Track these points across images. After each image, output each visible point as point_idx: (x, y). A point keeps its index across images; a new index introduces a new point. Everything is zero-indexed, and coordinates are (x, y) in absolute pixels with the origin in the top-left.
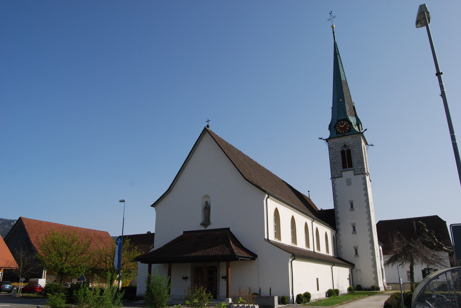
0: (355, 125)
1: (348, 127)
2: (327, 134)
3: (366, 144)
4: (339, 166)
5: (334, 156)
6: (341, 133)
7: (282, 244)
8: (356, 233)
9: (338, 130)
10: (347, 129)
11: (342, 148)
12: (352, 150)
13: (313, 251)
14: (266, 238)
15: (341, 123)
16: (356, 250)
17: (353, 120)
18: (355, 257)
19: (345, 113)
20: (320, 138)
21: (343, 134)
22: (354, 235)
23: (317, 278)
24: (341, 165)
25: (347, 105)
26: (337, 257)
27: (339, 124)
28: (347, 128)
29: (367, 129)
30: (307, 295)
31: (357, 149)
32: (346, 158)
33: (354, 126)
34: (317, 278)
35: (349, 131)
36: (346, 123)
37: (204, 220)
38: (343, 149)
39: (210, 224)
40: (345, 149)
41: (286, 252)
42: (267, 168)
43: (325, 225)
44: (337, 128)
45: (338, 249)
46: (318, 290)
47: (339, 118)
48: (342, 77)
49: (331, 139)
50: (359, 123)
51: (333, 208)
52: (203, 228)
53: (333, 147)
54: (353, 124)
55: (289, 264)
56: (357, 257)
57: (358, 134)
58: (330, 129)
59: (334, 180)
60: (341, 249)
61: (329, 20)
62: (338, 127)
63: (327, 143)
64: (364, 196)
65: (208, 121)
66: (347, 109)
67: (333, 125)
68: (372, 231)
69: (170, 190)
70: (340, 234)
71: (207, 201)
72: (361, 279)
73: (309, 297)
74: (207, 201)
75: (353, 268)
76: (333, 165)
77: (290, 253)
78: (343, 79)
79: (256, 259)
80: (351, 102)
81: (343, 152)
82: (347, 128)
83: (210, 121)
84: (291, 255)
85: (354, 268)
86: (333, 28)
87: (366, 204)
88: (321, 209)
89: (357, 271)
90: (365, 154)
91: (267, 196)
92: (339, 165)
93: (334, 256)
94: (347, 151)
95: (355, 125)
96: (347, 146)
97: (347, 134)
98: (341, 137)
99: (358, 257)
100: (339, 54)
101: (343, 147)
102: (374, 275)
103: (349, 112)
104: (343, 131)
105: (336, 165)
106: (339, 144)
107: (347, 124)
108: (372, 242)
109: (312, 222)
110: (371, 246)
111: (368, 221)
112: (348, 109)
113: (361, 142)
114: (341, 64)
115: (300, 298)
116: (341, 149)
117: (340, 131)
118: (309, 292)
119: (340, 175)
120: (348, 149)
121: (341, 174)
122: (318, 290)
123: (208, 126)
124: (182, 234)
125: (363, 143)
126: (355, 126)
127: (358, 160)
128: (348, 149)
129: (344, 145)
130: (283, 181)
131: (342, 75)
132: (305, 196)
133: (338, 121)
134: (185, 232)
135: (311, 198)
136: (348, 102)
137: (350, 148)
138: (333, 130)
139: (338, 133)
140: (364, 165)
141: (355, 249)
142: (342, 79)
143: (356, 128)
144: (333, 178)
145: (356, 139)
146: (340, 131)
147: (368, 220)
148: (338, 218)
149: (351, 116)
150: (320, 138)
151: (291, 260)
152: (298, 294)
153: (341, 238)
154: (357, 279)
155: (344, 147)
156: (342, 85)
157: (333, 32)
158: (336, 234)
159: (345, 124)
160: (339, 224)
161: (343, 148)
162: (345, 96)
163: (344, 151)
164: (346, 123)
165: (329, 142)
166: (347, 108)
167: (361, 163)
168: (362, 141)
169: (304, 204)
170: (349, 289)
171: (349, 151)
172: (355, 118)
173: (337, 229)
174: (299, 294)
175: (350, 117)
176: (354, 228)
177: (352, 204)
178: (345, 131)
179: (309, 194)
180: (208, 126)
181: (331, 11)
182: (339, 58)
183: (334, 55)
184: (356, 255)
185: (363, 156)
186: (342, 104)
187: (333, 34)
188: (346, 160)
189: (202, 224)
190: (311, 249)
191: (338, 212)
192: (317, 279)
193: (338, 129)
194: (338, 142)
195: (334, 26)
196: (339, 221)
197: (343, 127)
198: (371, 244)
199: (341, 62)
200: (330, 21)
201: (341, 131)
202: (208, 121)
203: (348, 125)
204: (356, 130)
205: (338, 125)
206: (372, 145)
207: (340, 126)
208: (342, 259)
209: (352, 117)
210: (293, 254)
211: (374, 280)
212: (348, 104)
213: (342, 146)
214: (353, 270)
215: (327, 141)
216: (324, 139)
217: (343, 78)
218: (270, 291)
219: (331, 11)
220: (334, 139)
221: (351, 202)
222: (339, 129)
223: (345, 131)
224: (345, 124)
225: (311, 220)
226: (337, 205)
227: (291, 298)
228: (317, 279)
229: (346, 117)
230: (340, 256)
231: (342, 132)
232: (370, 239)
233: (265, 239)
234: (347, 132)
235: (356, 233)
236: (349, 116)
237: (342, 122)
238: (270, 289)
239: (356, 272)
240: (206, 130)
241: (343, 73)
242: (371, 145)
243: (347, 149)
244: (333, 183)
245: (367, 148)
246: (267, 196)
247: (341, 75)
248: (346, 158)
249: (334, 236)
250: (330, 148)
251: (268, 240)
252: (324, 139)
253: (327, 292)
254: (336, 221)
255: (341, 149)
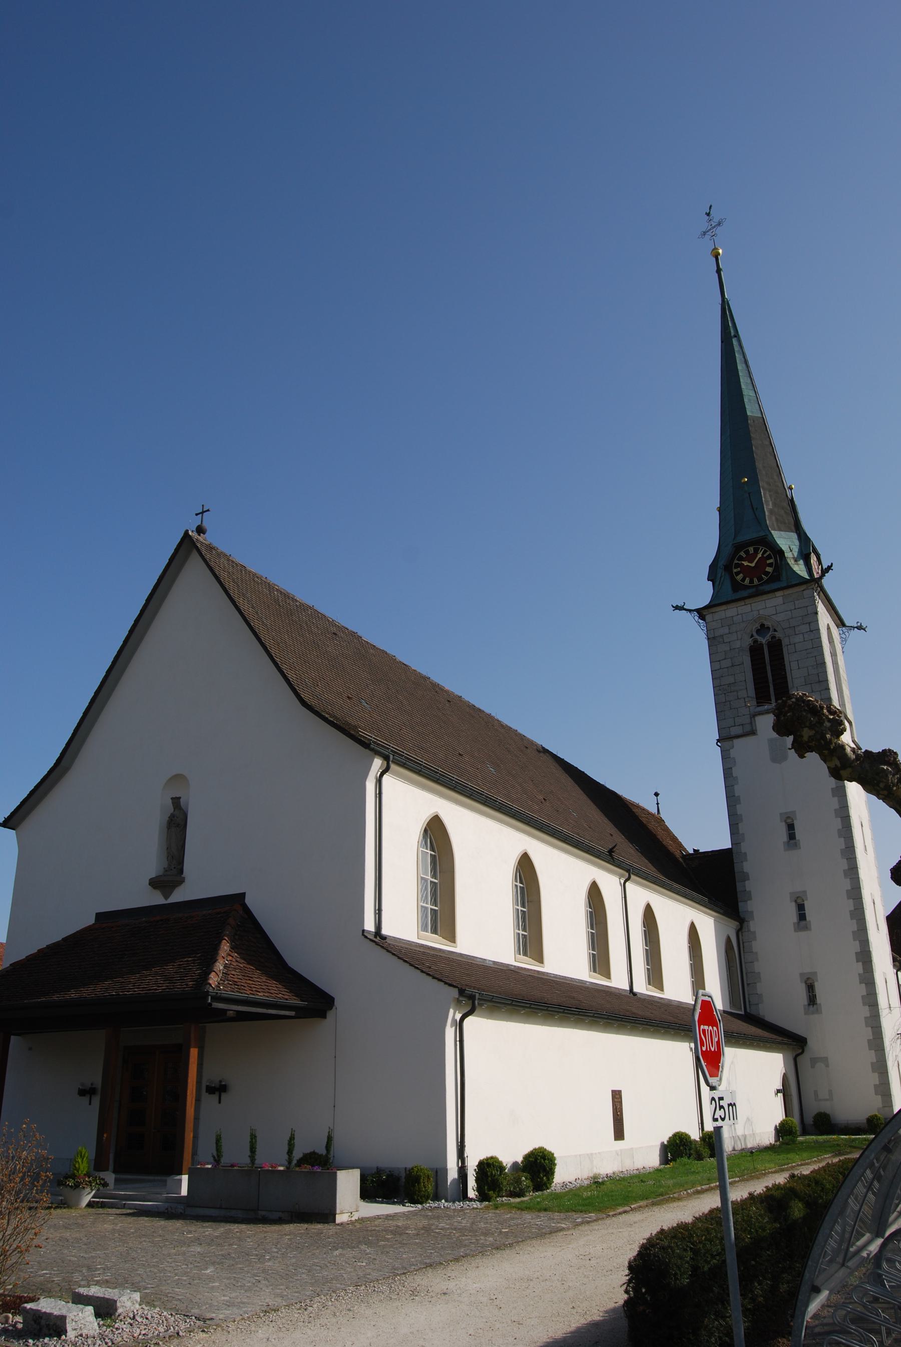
0: (794, 558)
1: (770, 565)
2: (703, 594)
3: (840, 623)
4: (744, 698)
5: (727, 663)
6: (746, 587)
7: (461, 955)
8: (807, 928)
9: (739, 577)
10: (767, 573)
11: (752, 636)
12: (785, 642)
13: (628, 988)
14: (369, 925)
15: (747, 552)
16: (811, 988)
17: (786, 542)
18: (806, 1014)
19: (760, 521)
20: (677, 608)
21: (754, 590)
22: (803, 934)
23: (613, 1091)
24: (752, 692)
25: (768, 495)
26: (742, 1013)
27: (741, 559)
28: (769, 569)
29: (832, 564)
30: (536, 1159)
31: (801, 636)
32: (768, 668)
33: (791, 562)
34: (613, 1091)
35: (775, 577)
36: (765, 552)
37: (166, 866)
38: (755, 641)
39: (182, 881)
40: (763, 640)
41: (435, 981)
42: (473, 701)
43: (685, 896)
44: (735, 570)
45: (748, 984)
46: (619, 1134)
47: (741, 539)
48: (747, 407)
49: (713, 610)
50: (807, 550)
51: (727, 844)
52: (158, 899)
53: (722, 636)
54: (788, 555)
55: (450, 1033)
56: (813, 1013)
57: (804, 587)
58: (712, 577)
59: (727, 744)
60: (758, 984)
61: (704, 233)
62: (737, 566)
63: (701, 621)
64: (833, 796)
65: (202, 513)
66: (768, 507)
67: (721, 563)
68: (864, 919)
69: (63, 763)
70: (754, 932)
71: (180, 798)
72: (830, 1092)
73: (545, 1170)
74: (180, 798)
75: (801, 1051)
76: (725, 694)
77: (450, 985)
78: (752, 412)
79: (330, 1014)
80: (780, 485)
81: (755, 651)
82: (769, 569)
83: (208, 510)
84: (455, 993)
85: (803, 1052)
86: (716, 256)
87: (838, 823)
88: (694, 850)
89: (814, 1061)
90: (834, 655)
91: (377, 764)
92: (746, 696)
93: (729, 1010)
94: (770, 645)
95: (794, 558)
96: (768, 628)
97: (767, 588)
98: (747, 601)
99: (818, 1011)
100: (737, 335)
101: (755, 634)
102: (876, 1075)
103: (774, 518)
104: (755, 580)
105: (735, 693)
106: (743, 621)
107: (768, 553)
108: (865, 957)
109: (622, 882)
110: (861, 971)
111: (847, 884)
112: (771, 507)
113: (816, 613)
114: (744, 365)
115: (487, 1176)
116: (748, 642)
117: (743, 580)
118: (549, 1147)
119: (748, 728)
120: (773, 637)
121: (752, 723)
122: (619, 1134)
123: (200, 530)
124: (91, 921)
125: (824, 619)
126: (796, 561)
127: (809, 675)
128: (773, 637)
129: (758, 626)
130: (546, 751)
131: (749, 400)
132: (638, 806)
133: (738, 547)
134: (99, 916)
135: (663, 815)
136: (768, 484)
137: (777, 635)
138: (722, 579)
139: (736, 586)
140: (828, 689)
141: (806, 983)
142: (749, 413)
143: (800, 569)
144: (725, 739)
145: (797, 602)
146: (743, 580)
147: (848, 880)
148: (746, 877)
149: (780, 530)
150: (677, 608)
151: (458, 1016)
152: (483, 1156)
153: (757, 946)
154: (816, 1093)
155: (758, 631)
156: (748, 432)
157: (719, 271)
158: (739, 932)
159: (760, 555)
160: (748, 896)
161: (756, 636)
162: (759, 465)
163: (762, 644)
164: (765, 552)
165: (708, 618)
166: (768, 505)
167: (819, 682)
168: (821, 608)
169: (616, 826)
170: (782, 1131)
171: (776, 646)
172: (794, 536)
173: (742, 916)
174: (487, 1159)
175: (775, 534)
176: (801, 908)
177: (791, 827)
178: (762, 579)
179: (658, 804)
180: (200, 530)
181: (711, 207)
182: (736, 348)
183: (722, 342)
184: (809, 1005)
185: (823, 659)
186: (749, 494)
187: (717, 275)
188: (767, 677)
189: (155, 883)
190: (618, 981)
191: (745, 853)
192: (617, 1096)
193: (738, 574)
194: (740, 616)
195: (720, 251)
196: (749, 885)
197: (753, 565)
198: (860, 964)
199: (747, 366)
200: (707, 237)
201: (747, 581)
202: (202, 513)
203: (769, 557)
204: (799, 572)
205: (738, 560)
206: (860, 628)
207: (746, 563)
208: (764, 1020)
209: (782, 533)
210: (462, 992)
211: (876, 1094)
212: (770, 491)
213: (752, 631)
214: (799, 1059)
215: (702, 617)
216: (690, 611)
217: (751, 410)
218: (253, 1150)
219: (711, 207)
220: (724, 607)
221: (788, 817)
222: (741, 575)
223: (760, 579)
224: (760, 555)
225: (621, 876)
226: (741, 832)
227: (452, 1174)
228: (617, 1096)
229: (762, 534)
230: (754, 1012)
231: (751, 581)
232: (856, 947)
233: (363, 931)
234: (767, 582)
235: (807, 928)
236: (775, 530)
237: (751, 550)
238: (253, 1137)
239: (813, 1067)
240: (187, 545)
241: (752, 393)
242: (856, 625)
243: (768, 637)
244: (725, 756)
245: (843, 636)
246: (377, 764)
247: (746, 400)
248: (768, 668)
249: (729, 941)
250: (713, 640)
251: (378, 939)
252: (690, 611)
253: (666, 1143)
254: (739, 887)
255: (750, 641)
